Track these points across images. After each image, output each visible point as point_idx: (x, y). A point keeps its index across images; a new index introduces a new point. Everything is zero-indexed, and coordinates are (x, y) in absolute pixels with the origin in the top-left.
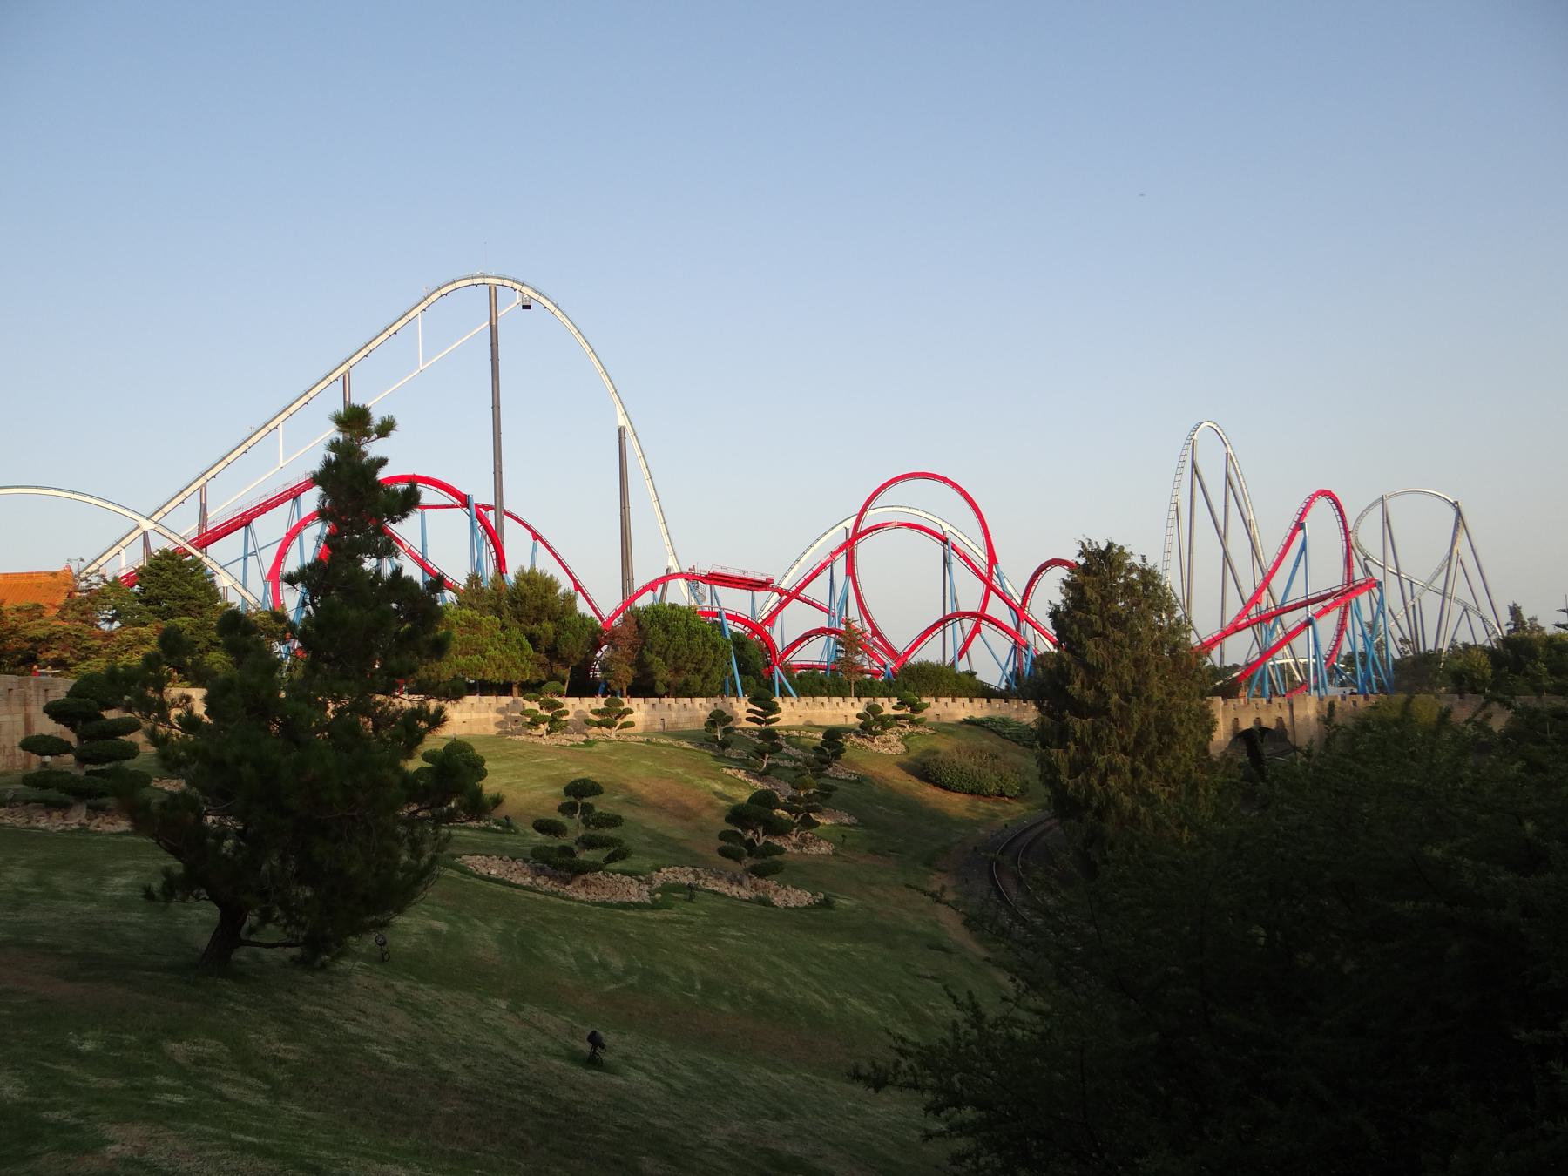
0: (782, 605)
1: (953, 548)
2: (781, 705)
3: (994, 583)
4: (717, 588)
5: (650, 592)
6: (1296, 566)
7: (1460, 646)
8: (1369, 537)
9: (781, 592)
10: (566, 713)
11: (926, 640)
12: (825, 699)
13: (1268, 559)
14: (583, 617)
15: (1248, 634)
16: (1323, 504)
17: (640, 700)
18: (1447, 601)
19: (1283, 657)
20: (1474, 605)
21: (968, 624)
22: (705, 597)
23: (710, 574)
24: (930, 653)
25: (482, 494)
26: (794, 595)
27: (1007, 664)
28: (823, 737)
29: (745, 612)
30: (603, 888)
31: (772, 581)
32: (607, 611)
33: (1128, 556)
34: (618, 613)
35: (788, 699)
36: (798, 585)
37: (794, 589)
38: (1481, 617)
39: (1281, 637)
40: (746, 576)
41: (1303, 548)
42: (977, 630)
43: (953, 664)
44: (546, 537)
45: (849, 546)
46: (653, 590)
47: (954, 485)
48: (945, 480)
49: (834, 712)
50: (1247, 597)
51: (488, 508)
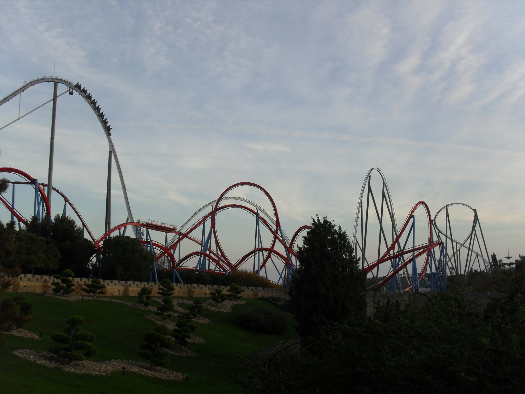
0: (180, 240)
1: (260, 218)
2: (175, 287)
3: (278, 235)
4: (149, 230)
6: (409, 234)
7: (474, 271)
8: (441, 222)
9: (179, 233)
10: (73, 285)
11: (245, 260)
12: (116, 282)
13: (399, 229)
14: (86, 240)
15: (388, 263)
16: (421, 207)
17: (109, 281)
18: (470, 252)
20: (481, 254)
21: (266, 254)
22: (144, 234)
24: (248, 266)
25: (42, 177)
26: (186, 235)
27: (282, 273)
28: (193, 303)
29: (162, 242)
30: (83, 367)
31: (176, 228)
32: (97, 237)
33: (333, 227)
34: (102, 239)
35: (179, 284)
36: (187, 231)
37: (186, 233)
38: (483, 259)
39: (403, 264)
40: (164, 225)
41: (413, 226)
42: (269, 256)
43: (257, 272)
44: (71, 201)
45: (213, 214)
47: (263, 189)
48: (258, 187)
49: (200, 292)
51: (44, 185)
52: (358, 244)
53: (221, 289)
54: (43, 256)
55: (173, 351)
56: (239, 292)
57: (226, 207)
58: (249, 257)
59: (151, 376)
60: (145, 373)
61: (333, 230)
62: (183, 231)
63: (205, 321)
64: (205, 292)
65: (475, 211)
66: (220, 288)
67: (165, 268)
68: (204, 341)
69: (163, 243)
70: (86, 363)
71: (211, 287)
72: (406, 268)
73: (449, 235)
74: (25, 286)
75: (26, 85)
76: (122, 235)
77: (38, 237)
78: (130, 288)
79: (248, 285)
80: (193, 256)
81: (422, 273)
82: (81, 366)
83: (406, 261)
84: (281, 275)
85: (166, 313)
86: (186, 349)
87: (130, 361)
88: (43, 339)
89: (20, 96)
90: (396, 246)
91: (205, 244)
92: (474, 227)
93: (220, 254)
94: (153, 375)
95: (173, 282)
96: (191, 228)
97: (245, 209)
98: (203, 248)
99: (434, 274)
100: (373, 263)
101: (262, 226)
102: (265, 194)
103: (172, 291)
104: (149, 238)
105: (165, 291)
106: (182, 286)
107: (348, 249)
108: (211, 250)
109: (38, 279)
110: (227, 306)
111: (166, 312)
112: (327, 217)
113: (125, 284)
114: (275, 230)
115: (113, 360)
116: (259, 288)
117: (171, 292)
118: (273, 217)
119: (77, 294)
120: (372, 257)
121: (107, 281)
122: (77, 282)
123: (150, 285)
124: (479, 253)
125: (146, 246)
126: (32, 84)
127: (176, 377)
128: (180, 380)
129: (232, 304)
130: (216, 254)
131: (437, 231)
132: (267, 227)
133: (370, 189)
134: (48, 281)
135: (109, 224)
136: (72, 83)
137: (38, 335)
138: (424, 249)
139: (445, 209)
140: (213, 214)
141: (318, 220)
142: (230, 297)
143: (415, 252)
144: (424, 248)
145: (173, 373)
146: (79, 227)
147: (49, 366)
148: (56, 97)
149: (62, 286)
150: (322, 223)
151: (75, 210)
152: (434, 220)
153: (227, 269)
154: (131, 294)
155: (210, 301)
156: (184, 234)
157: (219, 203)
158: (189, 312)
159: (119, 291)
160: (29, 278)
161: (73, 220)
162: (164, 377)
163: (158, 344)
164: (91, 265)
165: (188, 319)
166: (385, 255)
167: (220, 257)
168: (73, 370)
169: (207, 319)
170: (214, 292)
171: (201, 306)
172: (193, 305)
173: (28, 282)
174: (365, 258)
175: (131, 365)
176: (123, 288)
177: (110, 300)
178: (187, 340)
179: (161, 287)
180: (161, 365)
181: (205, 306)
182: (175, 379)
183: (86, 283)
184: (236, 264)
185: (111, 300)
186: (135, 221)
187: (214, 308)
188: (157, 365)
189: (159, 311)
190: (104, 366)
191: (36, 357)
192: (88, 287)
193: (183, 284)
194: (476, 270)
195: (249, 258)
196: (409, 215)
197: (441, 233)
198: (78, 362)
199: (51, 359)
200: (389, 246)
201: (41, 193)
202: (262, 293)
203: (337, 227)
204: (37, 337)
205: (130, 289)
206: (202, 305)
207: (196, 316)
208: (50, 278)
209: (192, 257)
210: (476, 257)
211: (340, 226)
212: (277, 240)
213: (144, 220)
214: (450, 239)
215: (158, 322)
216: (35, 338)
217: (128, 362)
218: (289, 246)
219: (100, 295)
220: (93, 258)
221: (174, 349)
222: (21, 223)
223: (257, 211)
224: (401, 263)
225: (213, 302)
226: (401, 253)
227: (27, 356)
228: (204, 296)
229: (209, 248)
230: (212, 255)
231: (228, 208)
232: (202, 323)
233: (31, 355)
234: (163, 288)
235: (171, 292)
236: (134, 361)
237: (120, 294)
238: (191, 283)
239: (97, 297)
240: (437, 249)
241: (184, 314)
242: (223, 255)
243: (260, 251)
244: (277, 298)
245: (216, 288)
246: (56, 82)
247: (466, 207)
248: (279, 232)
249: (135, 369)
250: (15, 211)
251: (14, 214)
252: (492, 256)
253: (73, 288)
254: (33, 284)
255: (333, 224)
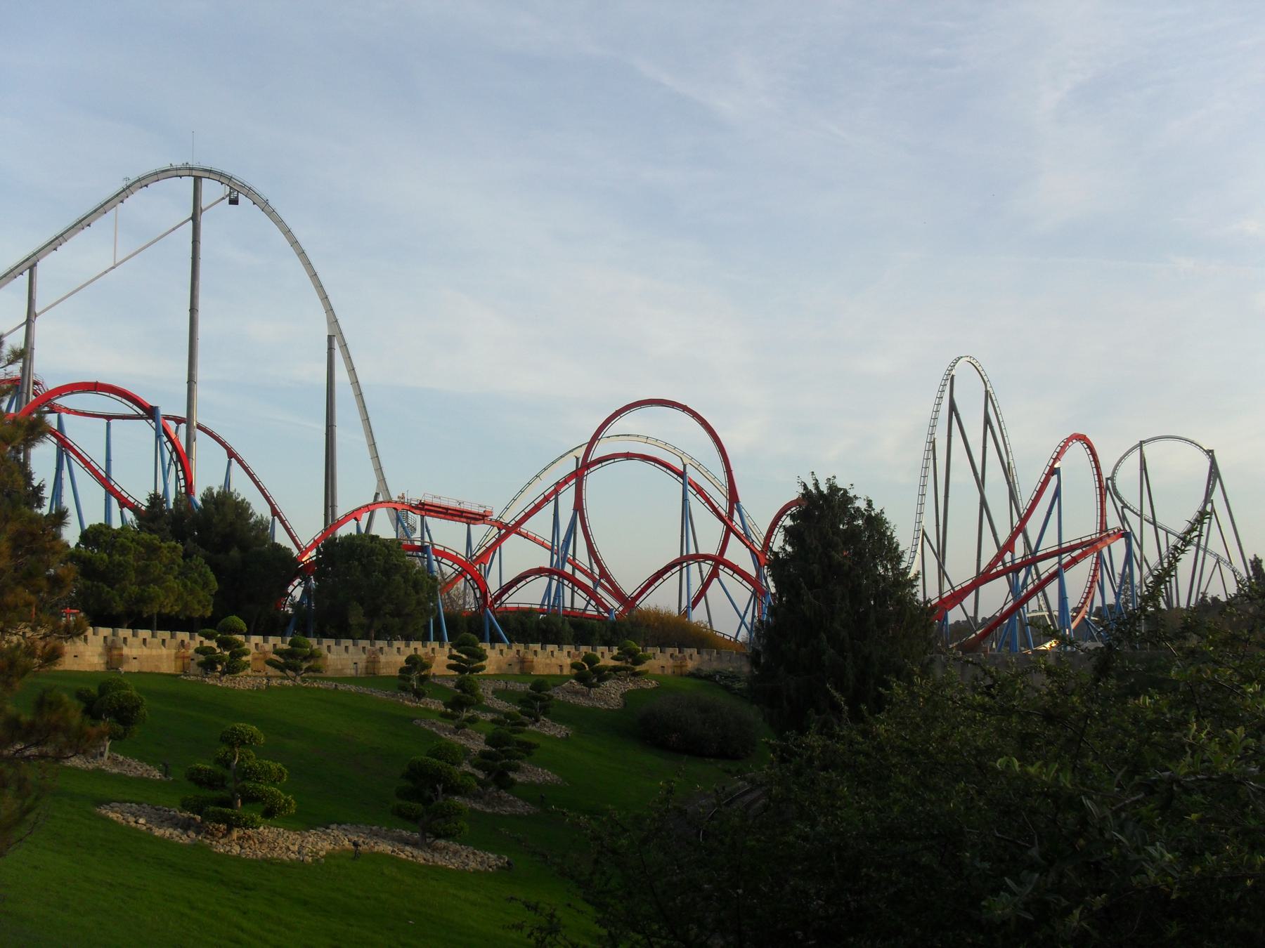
1: (690, 484)
4: (428, 519)
5: (353, 522)
6: (759, 540)
7: (1209, 601)
9: (501, 526)
10: (246, 653)
11: (656, 584)
12: (349, 642)
13: (1025, 500)
16: (1077, 448)
17: (332, 642)
18: (1201, 553)
19: (1033, 607)
22: (415, 529)
23: (421, 503)
24: (664, 599)
25: (172, 405)
26: (513, 529)
27: (746, 612)
32: (305, 540)
33: (851, 500)
36: (517, 519)
37: (513, 522)
41: (1057, 494)
44: (242, 455)
45: (578, 475)
46: (356, 519)
47: (695, 415)
48: (685, 409)
49: (548, 661)
50: (1002, 542)
51: (178, 421)
52: (929, 541)
53: (599, 655)
54: (176, 586)
55: (479, 802)
56: (638, 661)
57: (608, 460)
58: (665, 577)
59: (422, 861)
60: (407, 856)
61: (851, 508)
62: (508, 519)
63: (559, 730)
64: (559, 663)
65: (1210, 453)
66: (594, 653)
67: (467, 607)
68: (556, 777)
69: (461, 550)
70: (270, 835)
71: (573, 651)
72: (1045, 596)
73: (1147, 512)
74: (135, 658)
75: (128, 187)
76: (364, 532)
77: (165, 542)
78: (381, 656)
79: (663, 644)
80: (533, 577)
81: (1082, 607)
82: (256, 841)
83: (1043, 577)
84: (743, 618)
85: (465, 714)
86: (511, 798)
87: (374, 828)
88: (171, 778)
89: (116, 212)
90: (1019, 541)
91: (560, 549)
92: (1209, 493)
93: (597, 570)
94: (428, 861)
95: (482, 640)
96: (527, 511)
97: (653, 464)
98: (555, 557)
99: (1110, 607)
100: (963, 585)
101: (696, 503)
102: (701, 424)
103: (482, 660)
104: (427, 539)
105: (464, 661)
106: (505, 650)
107: (889, 554)
108: (577, 562)
109: (164, 641)
110: (612, 693)
111: (465, 710)
112: (834, 477)
113: (368, 647)
114: (726, 512)
115: (334, 826)
116: (688, 651)
117: (479, 664)
118: (722, 477)
119: (257, 674)
120: (961, 570)
121: (326, 642)
122: (256, 644)
123: (429, 649)
124: (1224, 555)
125: (421, 557)
126: (143, 184)
127: (482, 863)
128: (491, 870)
129: (623, 689)
130: (589, 570)
131: (1119, 505)
132: (706, 504)
133: (953, 408)
134: (189, 643)
135: (333, 506)
136: (235, 177)
137: (160, 771)
138: (1084, 549)
139: (1138, 451)
140: (578, 475)
141: (816, 485)
142: (618, 673)
143: (1064, 556)
144: (1085, 547)
145: (474, 854)
146: (259, 516)
147: (181, 841)
148: (199, 211)
149: (221, 656)
150: (825, 492)
151: (251, 476)
152: (1112, 478)
153: (612, 607)
154: (384, 672)
155: (571, 683)
156: (510, 525)
157: (593, 449)
158: (520, 711)
159: (355, 663)
160: (145, 640)
161: (244, 500)
162: (453, 864)
163: (440, 788)
164: (292, 605)
165: (514, 727)
166: (992, 565)
167: (598, 577)
168: (236, 850)
169: (564, 727)
170: (580, 661)
171: (548, 695)
172: (530, 693)
173: (160, 648)
174: (945, 573)
175: (375, 837)
176: (364, 656)
177: (334, 686)
178: (511, 775)
179: (455, 652)
180: (447, 836)
181: (558, 695)
182: (479, 867)
183: (278, 647)
184: (635, 594)
185: (336, 685)
186: (395, 498)
187: (581, 699)
188: (438, 836)
189: (449, 710)
190: (310, 840)
191: (152, 821)
192: (281, 657)
193: (508, 643)
194: (1215, 596)
195: (664, 580)
196: (1048, 468)
197: (1129, 509)
198: (250, 832)
199: (186, 826)
200: (1002, 543)
201: (170, 439)
202: (693, 660)
203: (862, 500)
204: (157, 775)
205: (383, 658)
206: (550, 693)
207: (537, 721)
208: (192, 638)
209: (528, 580)
210: (1215, 566)
211: (870, 498)
212: (732, 536)
213: (415, 496)
214: (1150, 522)
215: (446, 735)
216: (154, 776)
217: (371, 829)
218: (760, 549)
219: (311, 674)
220: (296, 587)
221: (481, 798)
222: (126, 510)
223: (685, 466)
224: (1033, 581)
225: (578, 686)
226: (1032, 560)
227: (131, 819)
228: (557, 671)
229: (571, 558)
230: (579, 576)
231: (613, 461)
232: (552, 735)
233: (141, 817)
234: (460, 654)
235: (479, 664)
236: (385, 828)
237: (359, 671)
238: (528, 643)
239: (304, 680)
240: (1119, 547)
241: (508, 715)
242: (604, 573)
243: (691, 562)
244: (730, 672)
245: (585, 652)
246: (198, 176)
247: (1187, 445)
248: (736, 516)
249: (385, 847)
250: (113, 483)
251: (110, 491)
252: (1251, 562)
253: (244, 658)
254: (154, 652)
255: (851, 494)
